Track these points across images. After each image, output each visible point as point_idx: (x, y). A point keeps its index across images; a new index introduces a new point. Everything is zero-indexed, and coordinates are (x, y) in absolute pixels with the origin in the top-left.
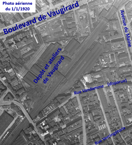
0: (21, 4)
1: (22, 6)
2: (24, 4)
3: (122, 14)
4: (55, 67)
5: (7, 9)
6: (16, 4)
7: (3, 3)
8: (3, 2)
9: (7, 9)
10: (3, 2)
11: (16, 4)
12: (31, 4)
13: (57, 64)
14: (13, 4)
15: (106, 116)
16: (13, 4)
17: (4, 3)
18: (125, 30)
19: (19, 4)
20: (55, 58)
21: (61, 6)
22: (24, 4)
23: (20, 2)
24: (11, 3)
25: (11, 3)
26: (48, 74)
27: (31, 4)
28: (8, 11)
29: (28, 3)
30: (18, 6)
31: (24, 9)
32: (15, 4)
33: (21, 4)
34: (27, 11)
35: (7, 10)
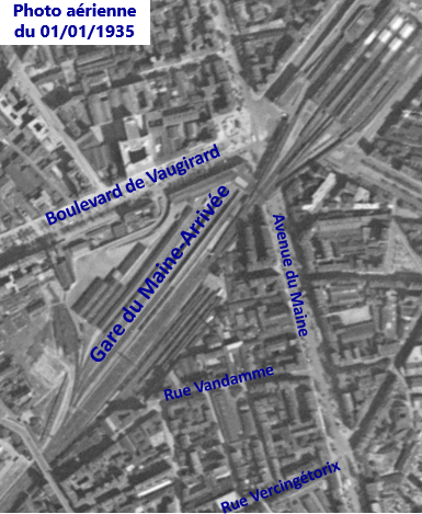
0: (91, 12)
1: (114, 21)
2: (101, 12)
3: (277, 228)
4: (181, 163)
5: (22, 30)
6: (72, 12)
7: (16, 12)
8: (16, 6)
9: (22, 31)
10: (16, 6)
11: (72, 12)
12: (132, 12)
13: (191, 160)
14: (56, 12)
15: (406, 172)
16: (56, 12)
17: (17, 9)
18: (137, 314)
19: (80, 12)
20: (88, 187)
21: (32, 101)
22: (101, 12)
23: (84, 7)
24: (48, 8)
25: (48, 8)
26: (152, 173)
27: (132, 12)
28: (25, 41)
29: (119, 9)
30: (77, 21)
31: (113, 31)
32: (64, 11)
33: (91, 12)
34: (125, 41)
35: (22, 35)
